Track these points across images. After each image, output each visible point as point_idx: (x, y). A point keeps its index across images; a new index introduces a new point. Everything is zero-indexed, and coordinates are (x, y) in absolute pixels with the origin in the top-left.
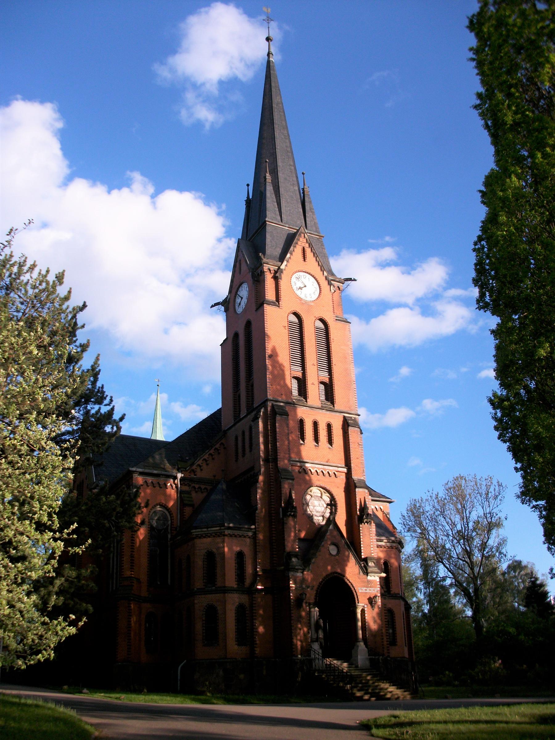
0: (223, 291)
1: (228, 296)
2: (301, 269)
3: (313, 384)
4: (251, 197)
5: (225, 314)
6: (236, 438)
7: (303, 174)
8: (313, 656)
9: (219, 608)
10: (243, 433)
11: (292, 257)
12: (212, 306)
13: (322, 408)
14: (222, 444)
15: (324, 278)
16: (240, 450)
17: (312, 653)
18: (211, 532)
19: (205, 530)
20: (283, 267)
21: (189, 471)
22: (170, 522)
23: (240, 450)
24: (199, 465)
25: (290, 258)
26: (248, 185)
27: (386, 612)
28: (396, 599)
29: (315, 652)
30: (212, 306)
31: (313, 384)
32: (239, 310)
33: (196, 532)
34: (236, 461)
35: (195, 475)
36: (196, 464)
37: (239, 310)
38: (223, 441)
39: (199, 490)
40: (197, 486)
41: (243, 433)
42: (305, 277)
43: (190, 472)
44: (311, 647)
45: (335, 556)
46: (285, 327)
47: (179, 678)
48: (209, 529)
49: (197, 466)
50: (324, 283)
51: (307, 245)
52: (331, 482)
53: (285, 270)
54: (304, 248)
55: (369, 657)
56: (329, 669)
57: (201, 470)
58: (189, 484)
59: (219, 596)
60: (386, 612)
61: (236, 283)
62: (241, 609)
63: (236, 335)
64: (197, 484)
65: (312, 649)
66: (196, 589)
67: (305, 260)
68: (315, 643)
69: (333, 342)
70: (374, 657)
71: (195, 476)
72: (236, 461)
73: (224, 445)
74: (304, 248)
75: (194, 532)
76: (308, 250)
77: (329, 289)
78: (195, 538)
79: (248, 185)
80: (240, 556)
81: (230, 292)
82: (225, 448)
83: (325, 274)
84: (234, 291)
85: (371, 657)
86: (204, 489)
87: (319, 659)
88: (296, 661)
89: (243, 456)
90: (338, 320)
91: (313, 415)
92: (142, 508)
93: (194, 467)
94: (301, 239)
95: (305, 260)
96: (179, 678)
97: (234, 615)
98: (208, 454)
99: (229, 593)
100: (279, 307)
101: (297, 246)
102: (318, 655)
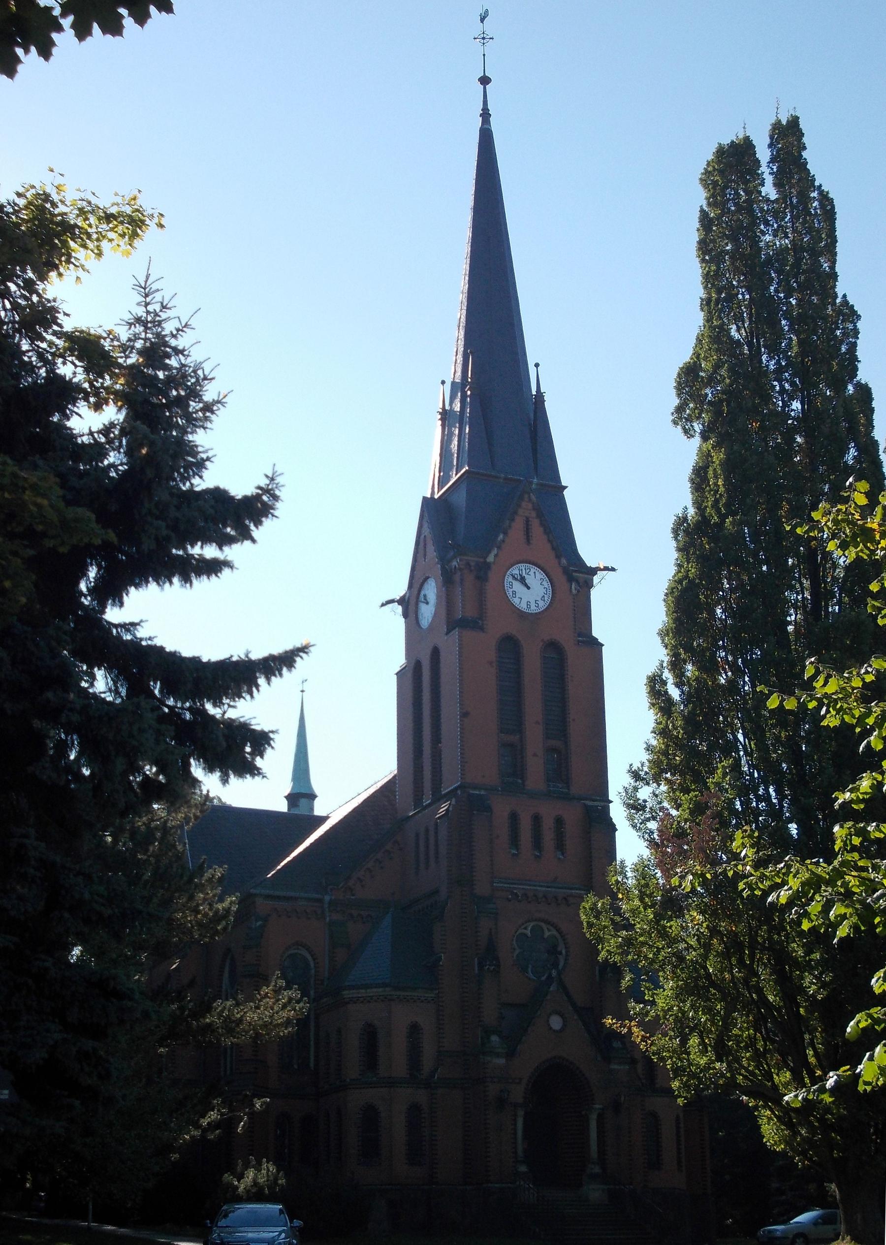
0: (400, 588)
1: (406, 593)
3: (535, 755)
6: (417, 835)
7: (537, 365)
10: (427, 830)
12: (383, 605)
16: (432, 853)
18: (372, 994)
19: (363, 991)
20: (491, 559)
22: (313, 972)
23: (432, 853)
25: (503, 541)
30: (383, 605)
35: (353, 895)
41: (427, 830)
42: (527, 571)
45: (557, 1031)
47: (279, 867)
48: (368, 990)
50: (561, 579)
51: (534, 514)
53: (494, 563)
62: (414, 1110)
66: (348, 1080)
71: (353, 897)
79: (443, 382)
80: (414, 1029)
83: (564, 561)
84: (416, 586)
92: (237, 902)
94: (524, 504)
96: (279, 867)
99: (397, 1087)
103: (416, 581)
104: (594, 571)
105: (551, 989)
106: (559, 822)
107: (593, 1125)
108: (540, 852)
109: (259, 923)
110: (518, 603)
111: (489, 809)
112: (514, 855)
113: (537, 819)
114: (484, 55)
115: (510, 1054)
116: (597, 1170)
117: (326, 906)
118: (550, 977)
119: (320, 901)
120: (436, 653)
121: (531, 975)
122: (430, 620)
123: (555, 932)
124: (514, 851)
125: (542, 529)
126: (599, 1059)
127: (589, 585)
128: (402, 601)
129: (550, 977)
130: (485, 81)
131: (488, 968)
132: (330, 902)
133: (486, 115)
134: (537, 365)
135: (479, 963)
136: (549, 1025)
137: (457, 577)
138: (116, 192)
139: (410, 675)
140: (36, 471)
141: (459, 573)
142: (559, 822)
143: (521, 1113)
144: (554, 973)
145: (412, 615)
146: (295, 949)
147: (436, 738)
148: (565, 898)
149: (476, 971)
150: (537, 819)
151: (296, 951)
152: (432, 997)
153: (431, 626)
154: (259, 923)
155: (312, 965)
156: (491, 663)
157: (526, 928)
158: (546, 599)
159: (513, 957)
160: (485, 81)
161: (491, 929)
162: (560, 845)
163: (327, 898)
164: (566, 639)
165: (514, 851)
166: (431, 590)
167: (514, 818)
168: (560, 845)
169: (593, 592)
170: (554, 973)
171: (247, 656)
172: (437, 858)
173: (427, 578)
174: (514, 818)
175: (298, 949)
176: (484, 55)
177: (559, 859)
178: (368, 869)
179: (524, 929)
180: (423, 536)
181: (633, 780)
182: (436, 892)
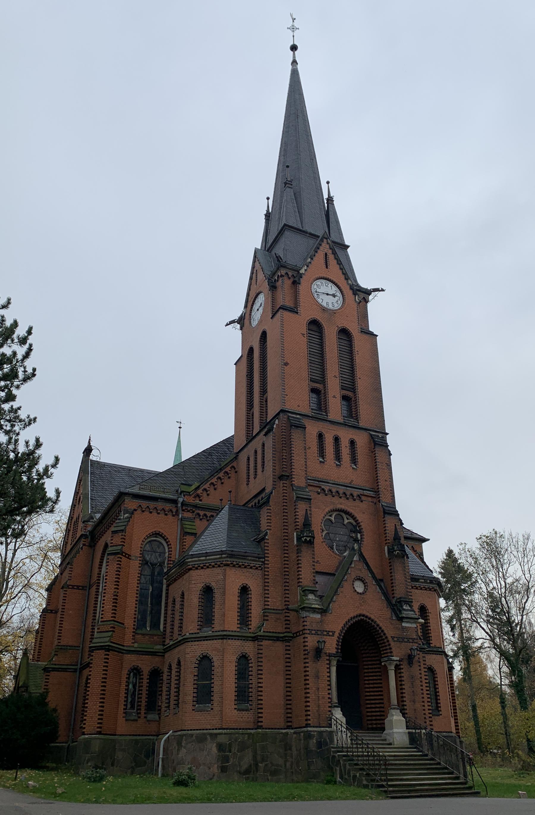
0: (238, 311)
2: (322, 275)
3: (334, 397)
4: (270, 211)
5: (240, 332)
7: (328, 183)
8: (334, 727)
9: (215, 659)
11: (312, 262)
12: (227, 325)
13: (345, 425)
14: (233, 467)
15: (348, 287)
17: (333, 722)
21: (193, 496)
22: (167, 554)
24: (205, 490)
26: (268, 199)
27: (426, 670)
28: (437, 654)
29: (337, 722)
30: (227, 325)
31: (334, 397)
32: (254, 324)
33: (192, 561)
34: (248, 484)
35: (201, 500)
36: (202, 488)
37: (254, 323)
38: (234, 464)
39: (205, 517)
40: (202, 513)
42: (327, 284)
43: (195, 497)
44: (332, 714)
46: (304, 334)
48: (208, 558)
49: (203, 490)
51: (330, 251)
52: (355, 507)
54: (326, 254)
55: (408, 730)
56: (355, 746)
57: (208, 495)
58: (192, 510)
59: (217, 643)
60: (426, 670)
61: (253, 295)
62: (243, 659)
63: (251, 350)
64: (201, 510)
65: (333, 717)
67: (327, 267)
68: (336, 709)
69: (358, 354)
70: (414, 731)
72: (248, 484)
73: (235, 469)
74: (326, 254)
75: (189, 562)
76: (331, 257)
77: (354, 298)
78: (190, 569)
79: (268, 199)
81: (246, 307)
82: (236, 472)
85: (411, 730)
86: (210, 517)
87: (342, 731)
88: (312, 733)
89: (255, 478)
90: (363, 331)
91: (334, 430)
93: (200, 491)
95: (327, 267)
97: (234, 668)
98: (216, 477)
100: (297, 313)
101: (319, 251)
102: (341, 726)
103: (249, 303)
104: (368, 292)
105: (355, 559)
106: (352, 443)
107: (392, 674)
109: (126, 515)
110: (321, 302)
112: (321, 462)
113: (337, 439)
114: (293, 36)
115: (323, 611)
117: (179, 505)
122: (259, 318)
123: (351, 521)
124: (321, 460)
125: (336, 261)
126: (394, 618)
130: (294, 48)
131: (306, 539)
132: (183, 504)
134: (328, 183)
136: (354, 588)
140: (163, 673)
142: (352, 443)
143: (334, 663)
146: (154, 537)
148: (359, 496)
149: (295, 542)
150: (337, 439)
151: (155, 538)
152: (259, 564)
154: (126, 515)
155: (167, 550)
157: (331, 516)
158: (339, 302)
159: (322, 536)
160: (294, 48)
161: (306, 510)
162: (354, 460)
163: (181, 500)
165: (321, 460)
167: (320, 436)
168: (354, 460)
169: (369, 305)
174: (320, 436)
175: (156, 537)
176: (293, 36)
177: (353, 468)
178: (212, 483)
179: (329, 516)
180: (255, 269)
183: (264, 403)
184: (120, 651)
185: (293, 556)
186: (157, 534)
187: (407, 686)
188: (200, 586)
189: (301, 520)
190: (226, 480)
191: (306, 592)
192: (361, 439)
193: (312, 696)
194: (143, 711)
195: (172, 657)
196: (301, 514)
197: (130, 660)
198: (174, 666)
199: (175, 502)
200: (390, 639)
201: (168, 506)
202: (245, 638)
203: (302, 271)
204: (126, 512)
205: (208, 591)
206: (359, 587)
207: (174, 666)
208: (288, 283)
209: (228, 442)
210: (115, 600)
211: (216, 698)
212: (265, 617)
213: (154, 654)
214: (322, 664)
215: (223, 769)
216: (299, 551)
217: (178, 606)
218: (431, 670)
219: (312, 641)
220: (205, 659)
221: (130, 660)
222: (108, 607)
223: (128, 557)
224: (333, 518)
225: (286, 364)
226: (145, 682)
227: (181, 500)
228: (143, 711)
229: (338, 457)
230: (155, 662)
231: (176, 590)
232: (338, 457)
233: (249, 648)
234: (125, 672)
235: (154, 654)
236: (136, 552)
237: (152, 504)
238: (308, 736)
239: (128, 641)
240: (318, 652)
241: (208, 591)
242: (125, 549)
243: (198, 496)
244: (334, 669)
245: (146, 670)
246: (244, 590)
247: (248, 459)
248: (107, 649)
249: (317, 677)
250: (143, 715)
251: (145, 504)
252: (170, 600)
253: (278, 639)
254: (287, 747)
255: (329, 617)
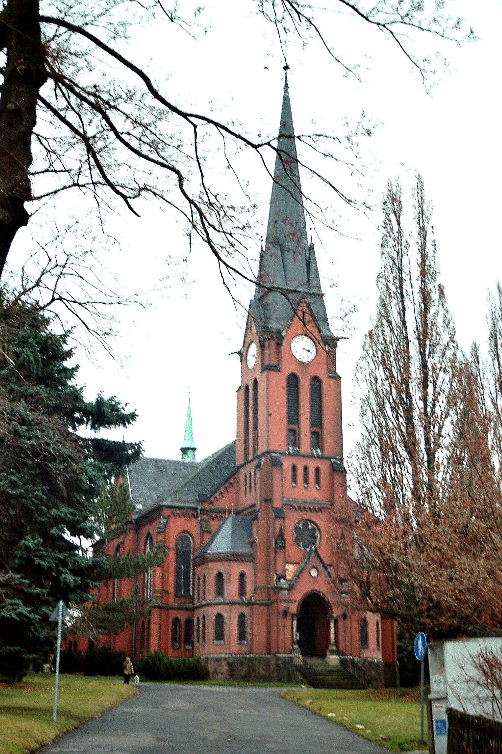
0: (239, 347)
40: (214, 515)
62: (242, 617)
100: (279, 371)
103: (246, 345)
104: (338, 339)
106: (317, 470)
108: (307, 484)
111: (281, 465)
113: (306, 469)
116: (334, 648)
118: (311, 549)
119: (196, 509)
120: (256, 382)
121: (302, 548)
123: (314, 526)
127: (335, 346)
128: (239, 353)
129: (311, 549)
132: (202, 510)
133: (286, 87)
135: (275, 541)
137: (266, 343)
138: (182, 449)
139: (243, 391)
141: (267, 341)
144: (313, 548)
145: (244, 362)
147: (256, 427)
150: (306, 469)
153: (254, 369)
156: (283, 388)
157: (299, 523)
162: (318, 482)
163: (199, 508)
164: (323, 375)
165: (294, 485)
166: (254, 349)
167: (294, 467)
168: (318, 482)
170: (313, 548)
171: (59, 27)
172: (255, 487)
173: (251, 343)
174: (294, 467)
181: (418, 381)
182: (254, 505)
183: (255, 449)
184: (167, 609)
185: (272, 554)
186: (185, 531)
187: (341, 633)
188: (215, 572)
189: (277, 531)
190: (230, 489)
191: (279, 578)
192: (324, 467)
193: (281, 637)
194: (182, 644)
195: (199, 613)
196: (278, 526)
197: (174, 614)
198: (201, 618)
199: (196, 509)
200: (332, 604)
201: (191, 512)
202: (243, 604)
203: (284, 334)
204: (164, 518)
205: (220, 576)
206: (314, 573)
207: (201, 618)
208: (273, 344)
209: (230, 450)
210: (163, 578)
211: (226, 637)
212: (255, 590)
213: (187, 609)
214: (289, 619)
215: (231, 676)
216: (276, 552)
217: (201, 582)
218: (365, 621)
219: (282, 607)
220: (219, 618)
221: (174, 614)
222: (158, 582)
223: (168, 548)
224: (301, 526)
225: (270, 415)
226: (183, 626)
227: (199, 508)
228: (182, 644)
229: (306, 481)
230: (188, 614)
231: (200, 571)
232: (306, 481)
233: (245, 610)
234: (171, 620)
235: (187, 609)
236: (172, 545)
237: (180, 512)
238: (278, 659)
239: (171, 601)
240: (285, 613)
241: (220, 576)
242: (166, 545)
243: (211, 502)
244: (295, 623)
245: (183, 619)
246: (242, 575)
247: (246, 476)
248: (160, 607)
249: (284, 627)
250: (183, 646)
251: (176, 511)
252: (196, 577)
253: (262, 604)
254: (268, 665)
255: (294, 592)
